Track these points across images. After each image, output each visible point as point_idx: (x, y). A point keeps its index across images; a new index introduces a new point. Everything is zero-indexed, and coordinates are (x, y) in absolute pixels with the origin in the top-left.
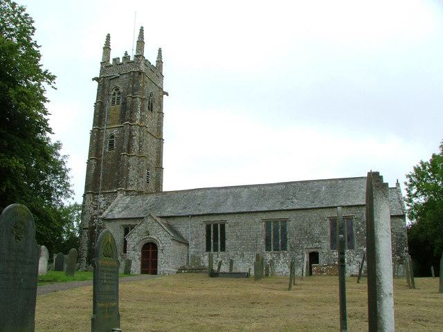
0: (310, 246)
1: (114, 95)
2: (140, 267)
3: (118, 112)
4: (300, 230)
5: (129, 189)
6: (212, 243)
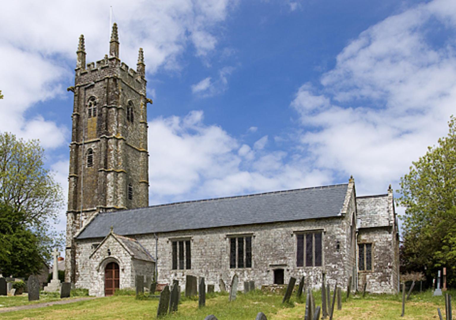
0: (275, 263)
1: (90, 106)
2: (103, 286)
4: (265, 245)
6: (178, 262)
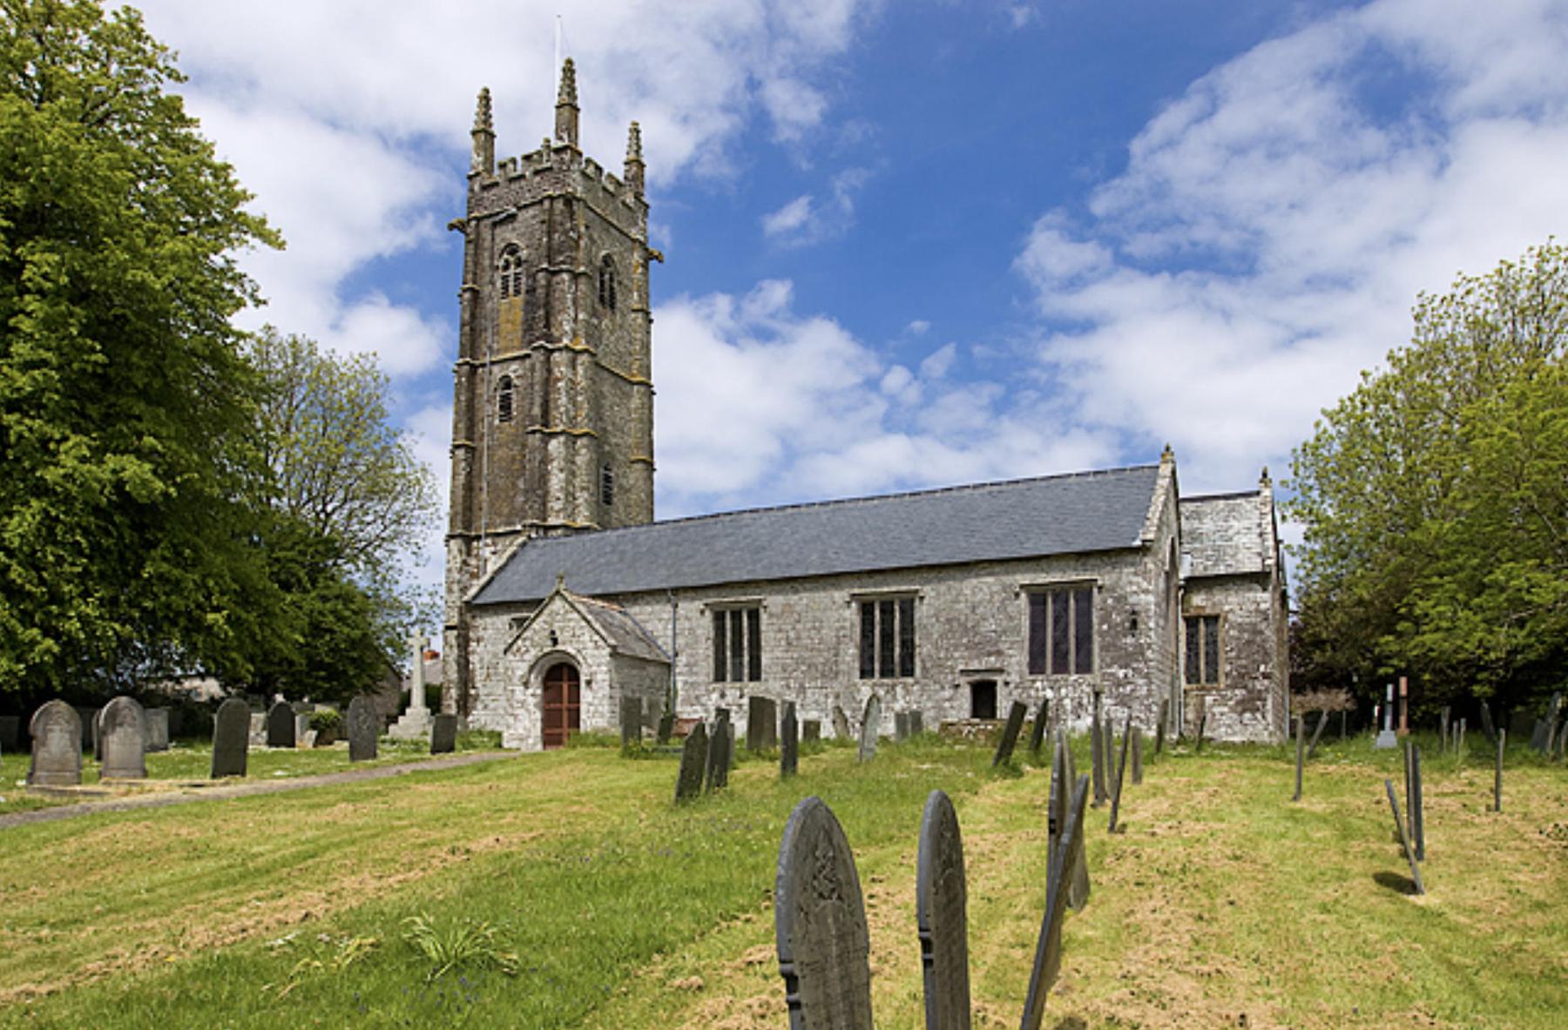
1: (506, 267)
2: (539, 725)
3: (519, 315)
4: (949, 621)
5: (552, 521)
6: (729, 662)
